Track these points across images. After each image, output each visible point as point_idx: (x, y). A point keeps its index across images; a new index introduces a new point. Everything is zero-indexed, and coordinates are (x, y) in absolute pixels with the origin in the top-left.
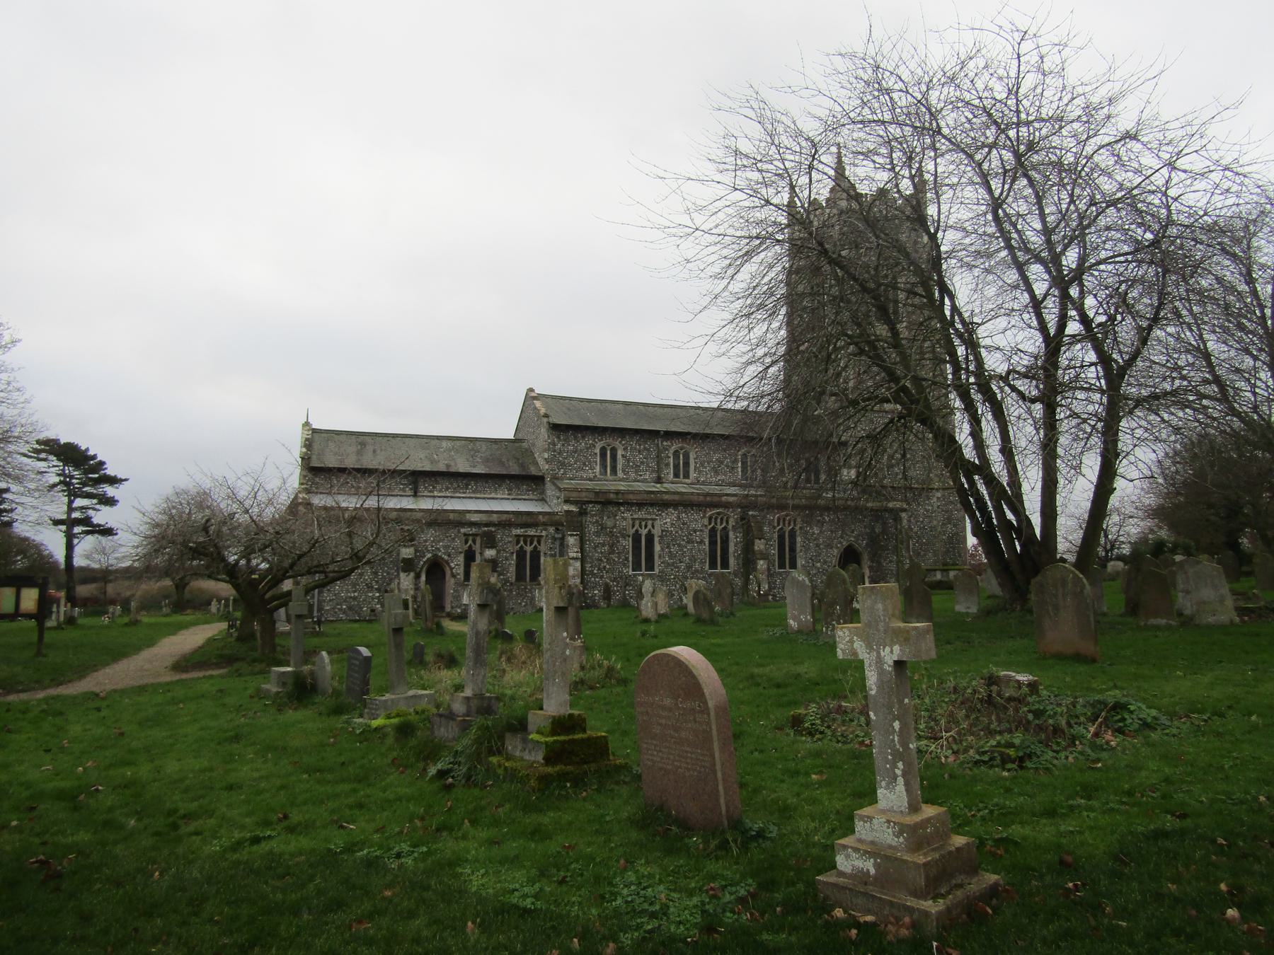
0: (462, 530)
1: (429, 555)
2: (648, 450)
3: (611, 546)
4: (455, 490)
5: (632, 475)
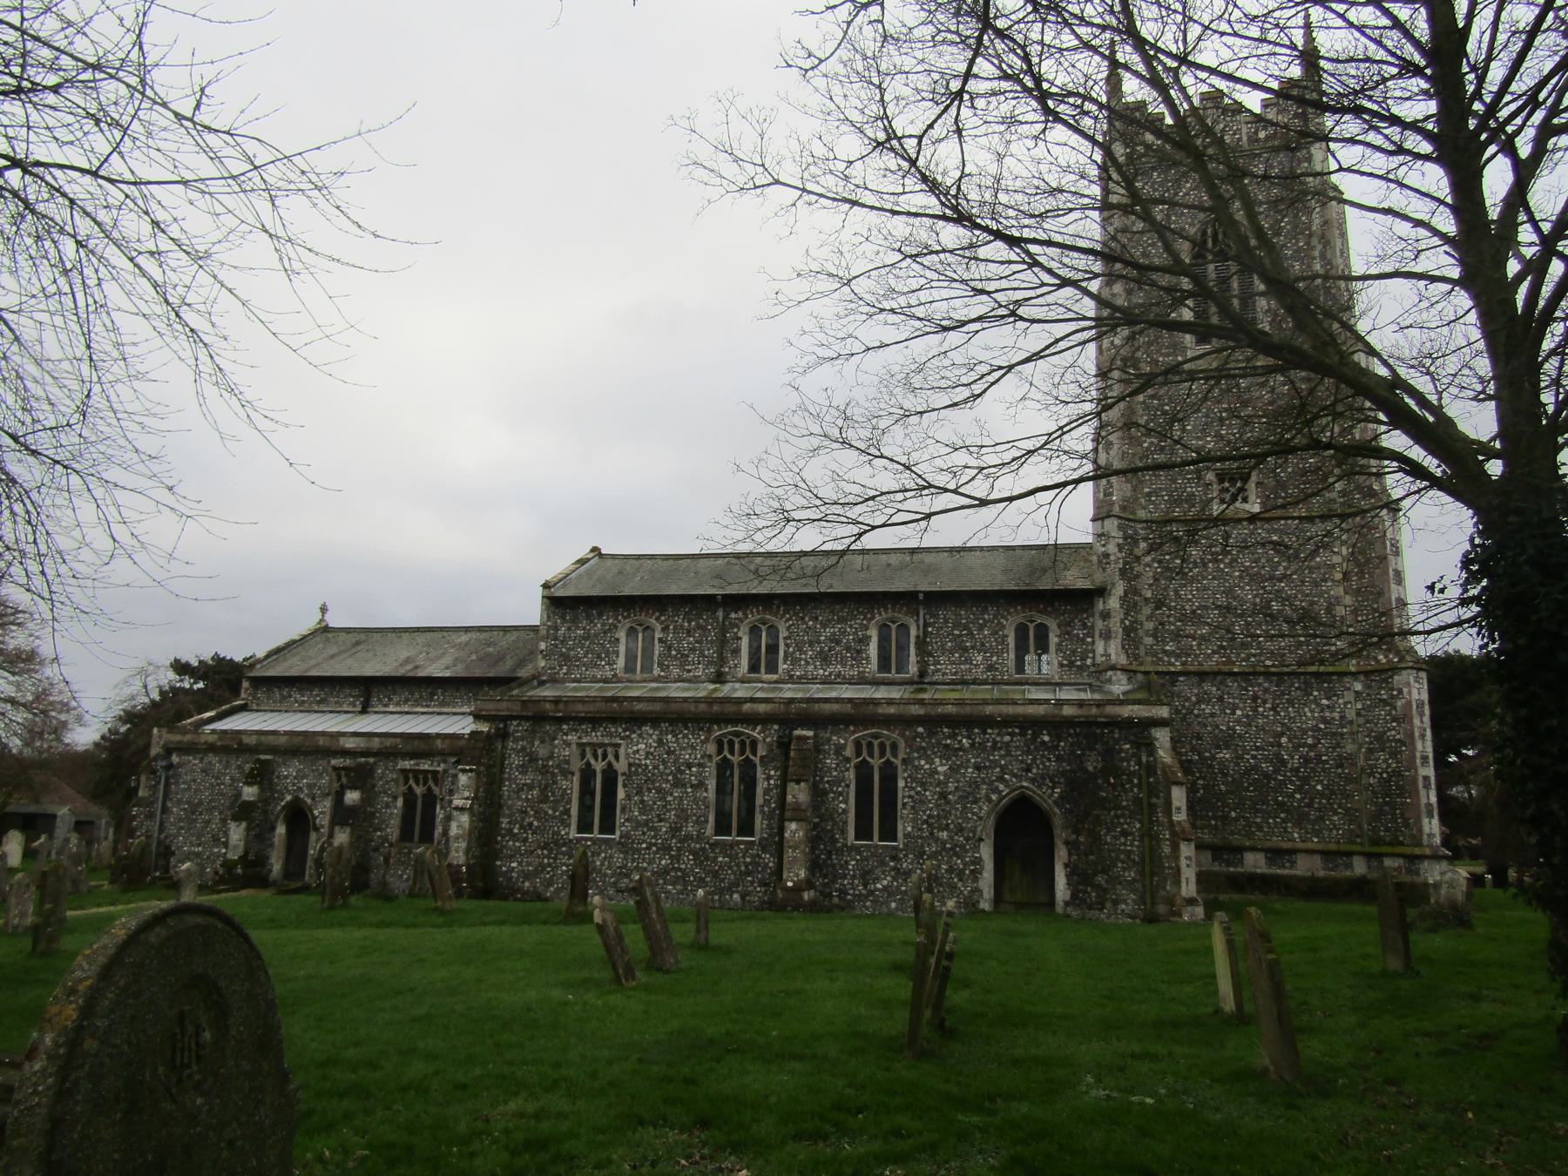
0: (333, 762)
1: (289, 798)
2: (703, 628)
3: (544, 790)
4: (417, 703)
5: (813, 676)
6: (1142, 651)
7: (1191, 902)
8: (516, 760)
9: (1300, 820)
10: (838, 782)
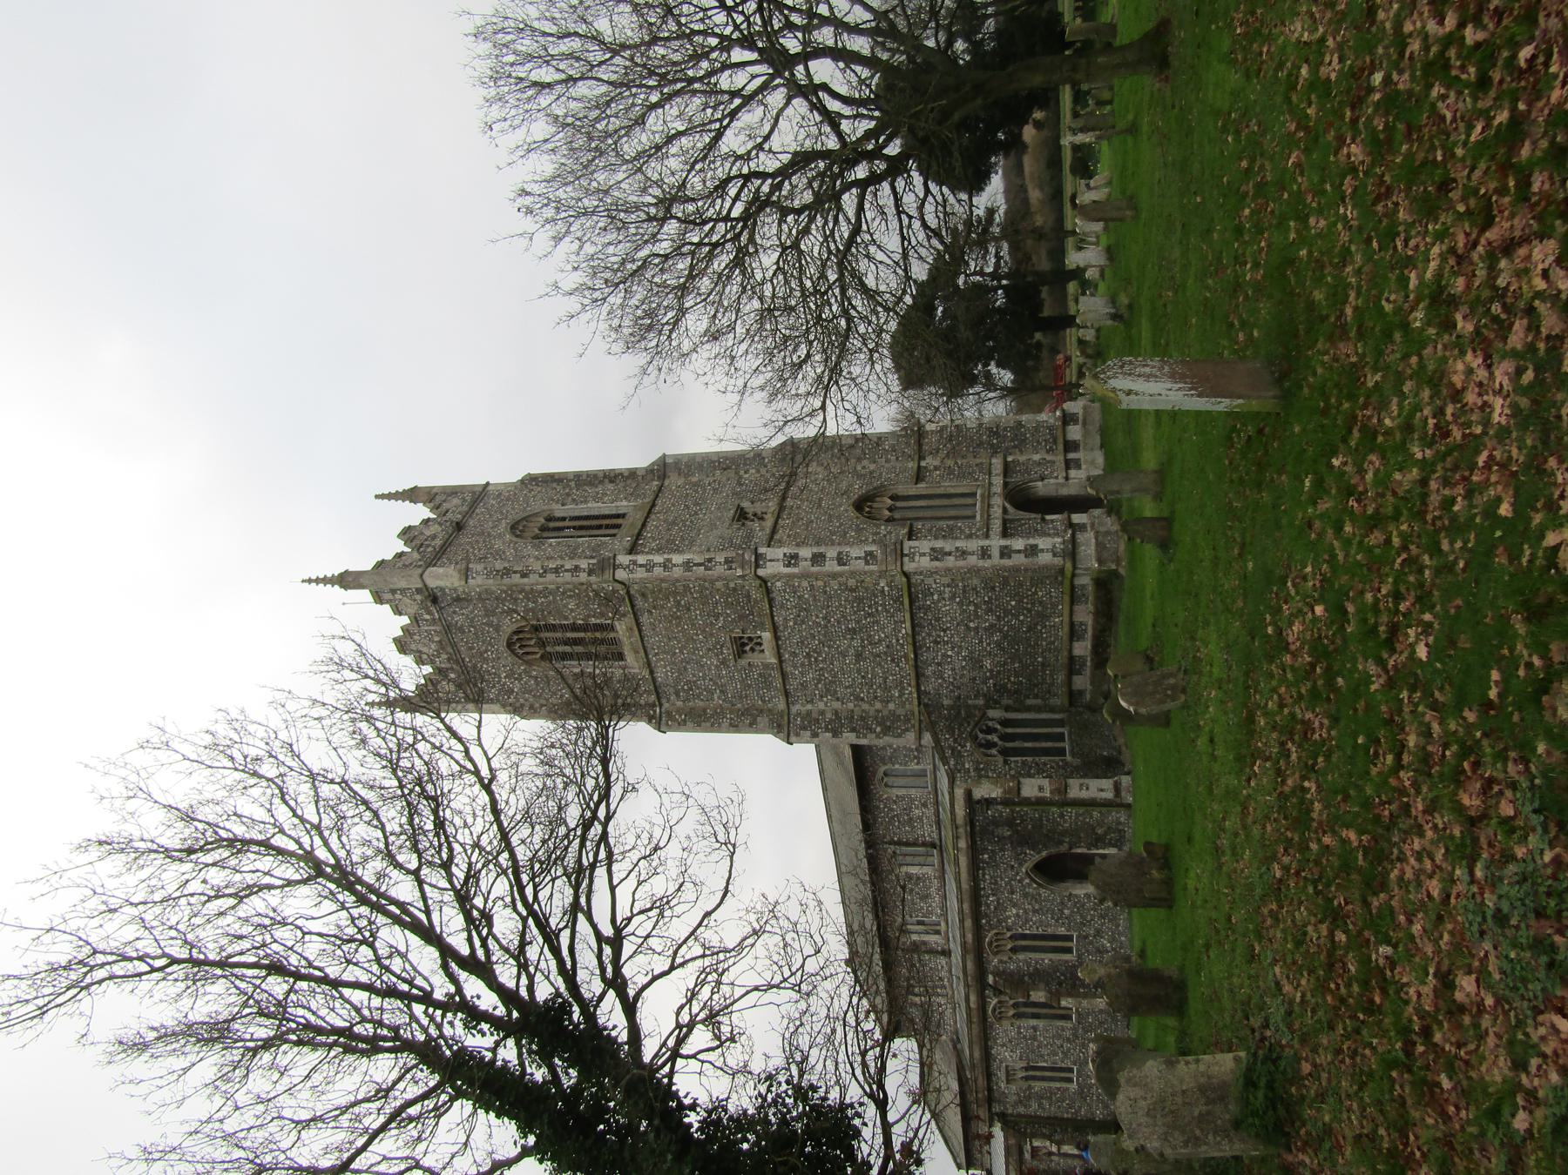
6: (900, 712)
7: (1117, 788)
8: (1021, 1110)
9: (1043, 617)
10: (1029, 965)
